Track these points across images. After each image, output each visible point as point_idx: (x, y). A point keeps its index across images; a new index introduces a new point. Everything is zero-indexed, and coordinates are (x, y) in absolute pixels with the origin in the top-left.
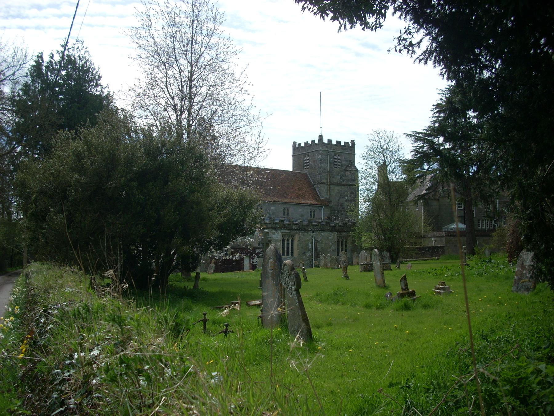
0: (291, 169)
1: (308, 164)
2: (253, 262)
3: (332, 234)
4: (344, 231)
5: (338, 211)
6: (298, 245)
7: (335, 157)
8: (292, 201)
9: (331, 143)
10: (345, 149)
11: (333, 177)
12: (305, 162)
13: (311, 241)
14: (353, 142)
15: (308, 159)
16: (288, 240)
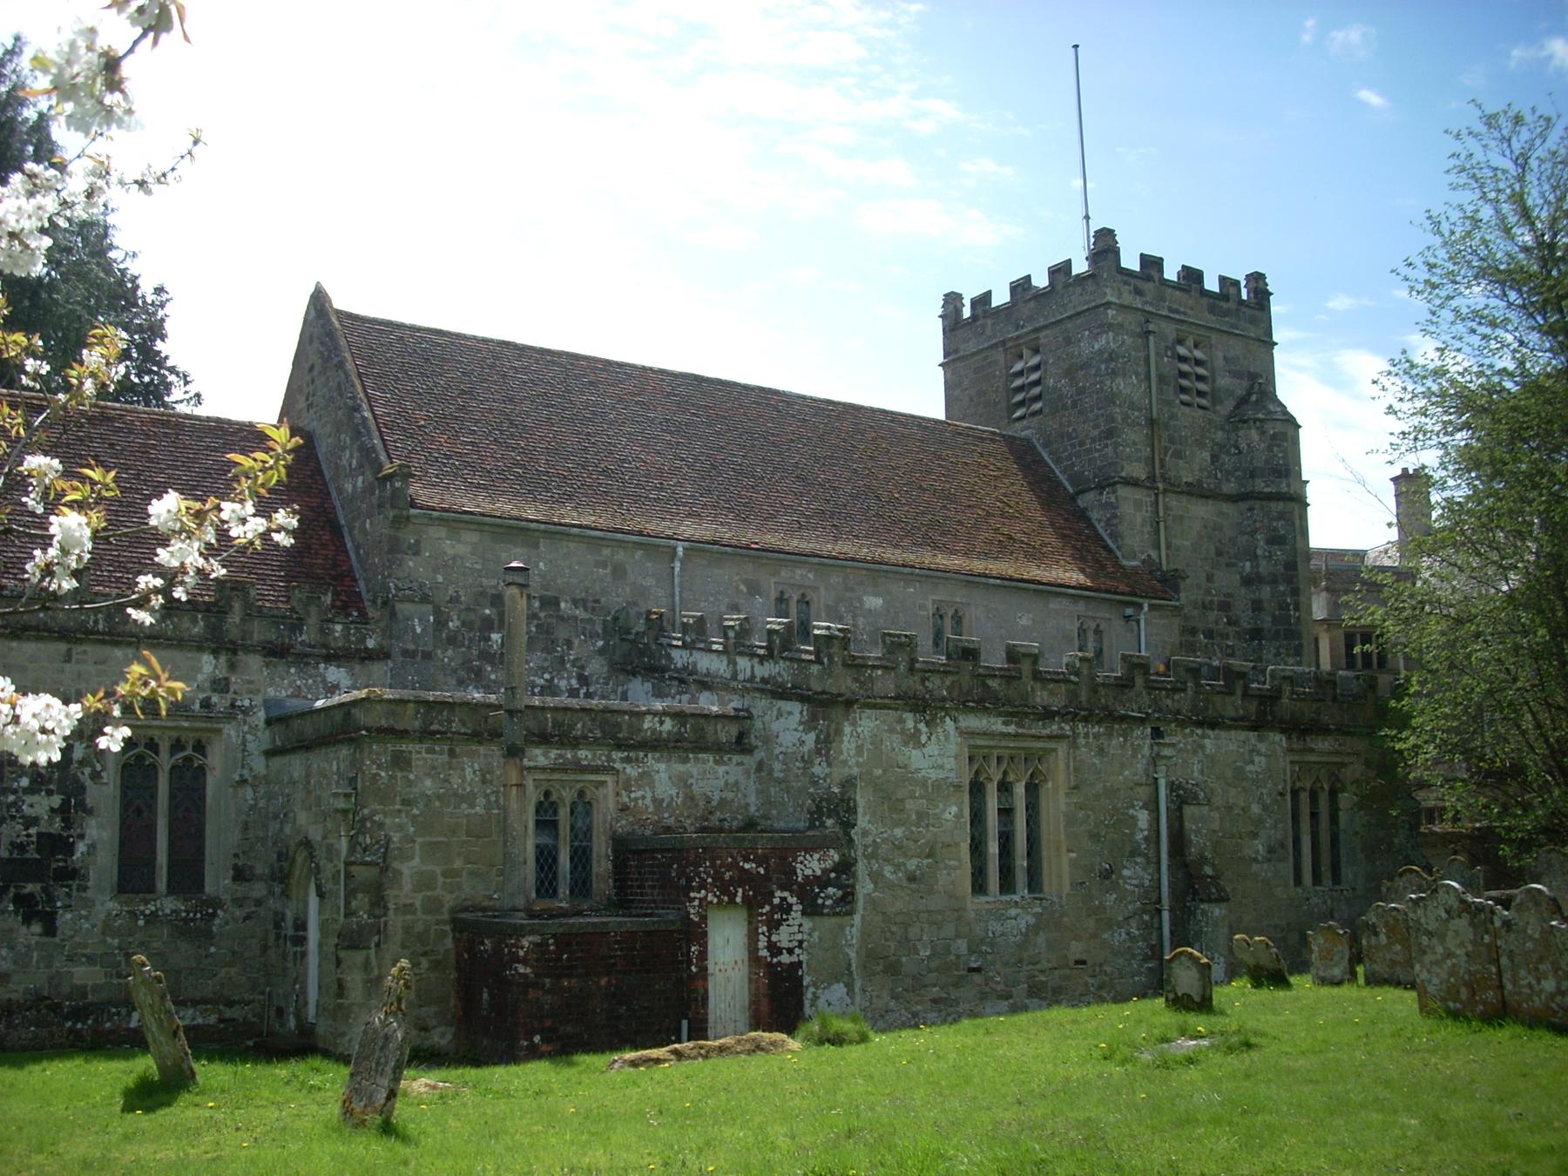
0: (940, 415)
1: (1036, 391)
2: (774, 949)
3: (1262, 747)
4: (1324, 731)
5: (1209, 634)
6: (1071, 820)
7: (1182, 350)
8: (978, 566)
9: (1156, 275)
10: (1227, 313)
11: (1178, 455)
12: (1018, 382)
13: (1144, 792)
14: (1257, 279)
15: (1036, 368)
16: (1005, 787)
